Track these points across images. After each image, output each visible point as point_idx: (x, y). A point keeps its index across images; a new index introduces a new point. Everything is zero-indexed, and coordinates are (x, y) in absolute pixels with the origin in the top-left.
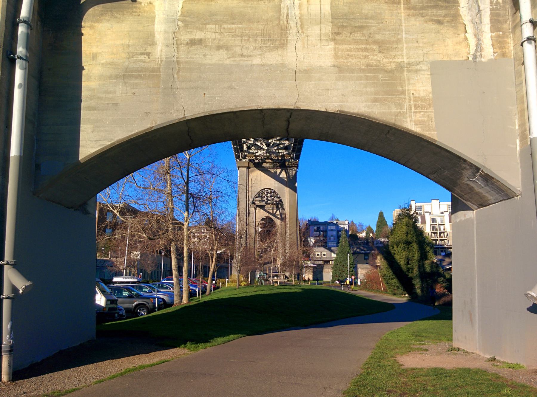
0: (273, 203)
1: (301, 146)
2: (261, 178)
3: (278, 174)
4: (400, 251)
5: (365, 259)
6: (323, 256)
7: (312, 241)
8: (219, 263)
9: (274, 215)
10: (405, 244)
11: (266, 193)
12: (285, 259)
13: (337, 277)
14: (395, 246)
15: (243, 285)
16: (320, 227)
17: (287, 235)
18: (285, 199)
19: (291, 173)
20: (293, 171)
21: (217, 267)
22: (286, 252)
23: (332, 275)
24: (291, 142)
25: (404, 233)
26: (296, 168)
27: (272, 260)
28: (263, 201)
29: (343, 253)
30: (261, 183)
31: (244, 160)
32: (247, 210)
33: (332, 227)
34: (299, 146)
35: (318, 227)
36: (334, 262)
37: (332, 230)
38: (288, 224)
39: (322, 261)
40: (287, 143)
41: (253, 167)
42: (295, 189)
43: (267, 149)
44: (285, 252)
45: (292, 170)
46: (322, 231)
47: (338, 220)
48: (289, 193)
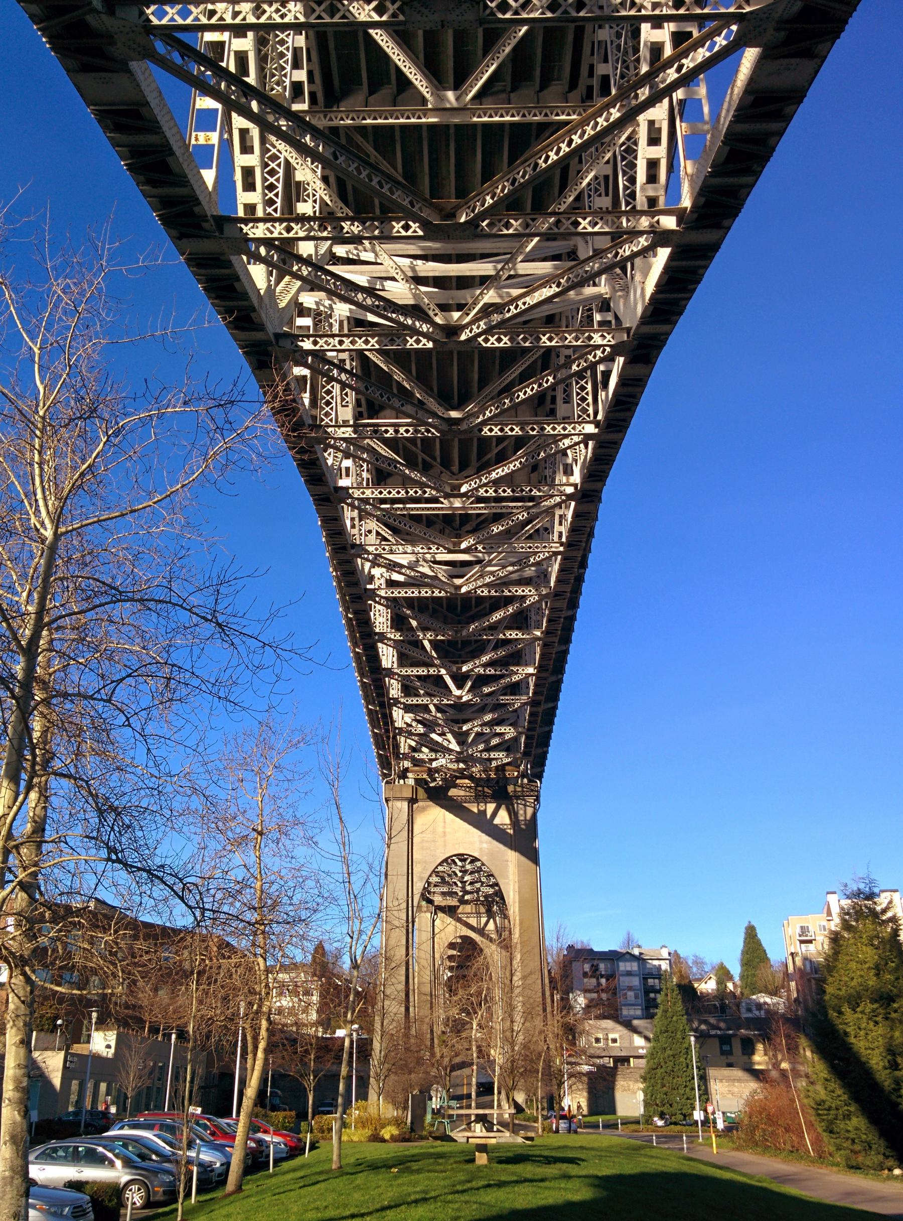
0: (477, 900)
1: (545, 749)
2: (444, 827)
3: (488, 816)
4: (863, 1026)
5: (723, 1053)
6: (611, 1044)
7: (580, 1001)
8: (321, 1066)
9: (481, 931)
10: (876, 1001)
11: (460, 874)
12: (513, 1050)
13: (657, 1105)
14: (846, 1009)
15: (387, 1137)
16: (598, 965)
17: (515, 978)
18: (508, 884)
19: (521, 812)
20: (528, 808)
21: (315, 1077)
22: (515, 1028)
23: (644, 1100)
24: (520, 730)
25: (869, 968)
26: (535, 800)
27: (475, 1055)
28: (452, 894)
29: (670, 1034)
30: (445, 841)
31: (402, 782)
32: (410, 909)
33: (628, 964)
34: (540, 751)
35: (592, 966)
36: (648, 1062)
37: (629, 974)
38: (519, 946)
39: (610, 1057)
40: (509, 732)
41: (423, 800)
42: (533, 856)
43: (458, 749)
44: (513, 1031)
45: (525, 805)
46: (602, 976)
47: (639, 947)
48: (519, 865)
